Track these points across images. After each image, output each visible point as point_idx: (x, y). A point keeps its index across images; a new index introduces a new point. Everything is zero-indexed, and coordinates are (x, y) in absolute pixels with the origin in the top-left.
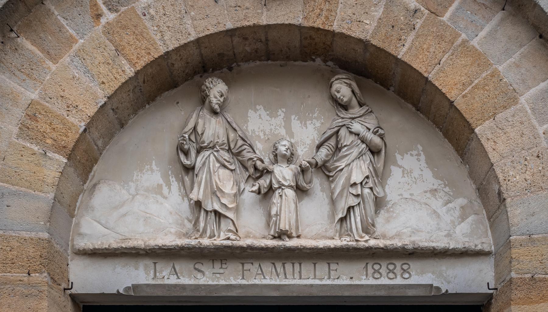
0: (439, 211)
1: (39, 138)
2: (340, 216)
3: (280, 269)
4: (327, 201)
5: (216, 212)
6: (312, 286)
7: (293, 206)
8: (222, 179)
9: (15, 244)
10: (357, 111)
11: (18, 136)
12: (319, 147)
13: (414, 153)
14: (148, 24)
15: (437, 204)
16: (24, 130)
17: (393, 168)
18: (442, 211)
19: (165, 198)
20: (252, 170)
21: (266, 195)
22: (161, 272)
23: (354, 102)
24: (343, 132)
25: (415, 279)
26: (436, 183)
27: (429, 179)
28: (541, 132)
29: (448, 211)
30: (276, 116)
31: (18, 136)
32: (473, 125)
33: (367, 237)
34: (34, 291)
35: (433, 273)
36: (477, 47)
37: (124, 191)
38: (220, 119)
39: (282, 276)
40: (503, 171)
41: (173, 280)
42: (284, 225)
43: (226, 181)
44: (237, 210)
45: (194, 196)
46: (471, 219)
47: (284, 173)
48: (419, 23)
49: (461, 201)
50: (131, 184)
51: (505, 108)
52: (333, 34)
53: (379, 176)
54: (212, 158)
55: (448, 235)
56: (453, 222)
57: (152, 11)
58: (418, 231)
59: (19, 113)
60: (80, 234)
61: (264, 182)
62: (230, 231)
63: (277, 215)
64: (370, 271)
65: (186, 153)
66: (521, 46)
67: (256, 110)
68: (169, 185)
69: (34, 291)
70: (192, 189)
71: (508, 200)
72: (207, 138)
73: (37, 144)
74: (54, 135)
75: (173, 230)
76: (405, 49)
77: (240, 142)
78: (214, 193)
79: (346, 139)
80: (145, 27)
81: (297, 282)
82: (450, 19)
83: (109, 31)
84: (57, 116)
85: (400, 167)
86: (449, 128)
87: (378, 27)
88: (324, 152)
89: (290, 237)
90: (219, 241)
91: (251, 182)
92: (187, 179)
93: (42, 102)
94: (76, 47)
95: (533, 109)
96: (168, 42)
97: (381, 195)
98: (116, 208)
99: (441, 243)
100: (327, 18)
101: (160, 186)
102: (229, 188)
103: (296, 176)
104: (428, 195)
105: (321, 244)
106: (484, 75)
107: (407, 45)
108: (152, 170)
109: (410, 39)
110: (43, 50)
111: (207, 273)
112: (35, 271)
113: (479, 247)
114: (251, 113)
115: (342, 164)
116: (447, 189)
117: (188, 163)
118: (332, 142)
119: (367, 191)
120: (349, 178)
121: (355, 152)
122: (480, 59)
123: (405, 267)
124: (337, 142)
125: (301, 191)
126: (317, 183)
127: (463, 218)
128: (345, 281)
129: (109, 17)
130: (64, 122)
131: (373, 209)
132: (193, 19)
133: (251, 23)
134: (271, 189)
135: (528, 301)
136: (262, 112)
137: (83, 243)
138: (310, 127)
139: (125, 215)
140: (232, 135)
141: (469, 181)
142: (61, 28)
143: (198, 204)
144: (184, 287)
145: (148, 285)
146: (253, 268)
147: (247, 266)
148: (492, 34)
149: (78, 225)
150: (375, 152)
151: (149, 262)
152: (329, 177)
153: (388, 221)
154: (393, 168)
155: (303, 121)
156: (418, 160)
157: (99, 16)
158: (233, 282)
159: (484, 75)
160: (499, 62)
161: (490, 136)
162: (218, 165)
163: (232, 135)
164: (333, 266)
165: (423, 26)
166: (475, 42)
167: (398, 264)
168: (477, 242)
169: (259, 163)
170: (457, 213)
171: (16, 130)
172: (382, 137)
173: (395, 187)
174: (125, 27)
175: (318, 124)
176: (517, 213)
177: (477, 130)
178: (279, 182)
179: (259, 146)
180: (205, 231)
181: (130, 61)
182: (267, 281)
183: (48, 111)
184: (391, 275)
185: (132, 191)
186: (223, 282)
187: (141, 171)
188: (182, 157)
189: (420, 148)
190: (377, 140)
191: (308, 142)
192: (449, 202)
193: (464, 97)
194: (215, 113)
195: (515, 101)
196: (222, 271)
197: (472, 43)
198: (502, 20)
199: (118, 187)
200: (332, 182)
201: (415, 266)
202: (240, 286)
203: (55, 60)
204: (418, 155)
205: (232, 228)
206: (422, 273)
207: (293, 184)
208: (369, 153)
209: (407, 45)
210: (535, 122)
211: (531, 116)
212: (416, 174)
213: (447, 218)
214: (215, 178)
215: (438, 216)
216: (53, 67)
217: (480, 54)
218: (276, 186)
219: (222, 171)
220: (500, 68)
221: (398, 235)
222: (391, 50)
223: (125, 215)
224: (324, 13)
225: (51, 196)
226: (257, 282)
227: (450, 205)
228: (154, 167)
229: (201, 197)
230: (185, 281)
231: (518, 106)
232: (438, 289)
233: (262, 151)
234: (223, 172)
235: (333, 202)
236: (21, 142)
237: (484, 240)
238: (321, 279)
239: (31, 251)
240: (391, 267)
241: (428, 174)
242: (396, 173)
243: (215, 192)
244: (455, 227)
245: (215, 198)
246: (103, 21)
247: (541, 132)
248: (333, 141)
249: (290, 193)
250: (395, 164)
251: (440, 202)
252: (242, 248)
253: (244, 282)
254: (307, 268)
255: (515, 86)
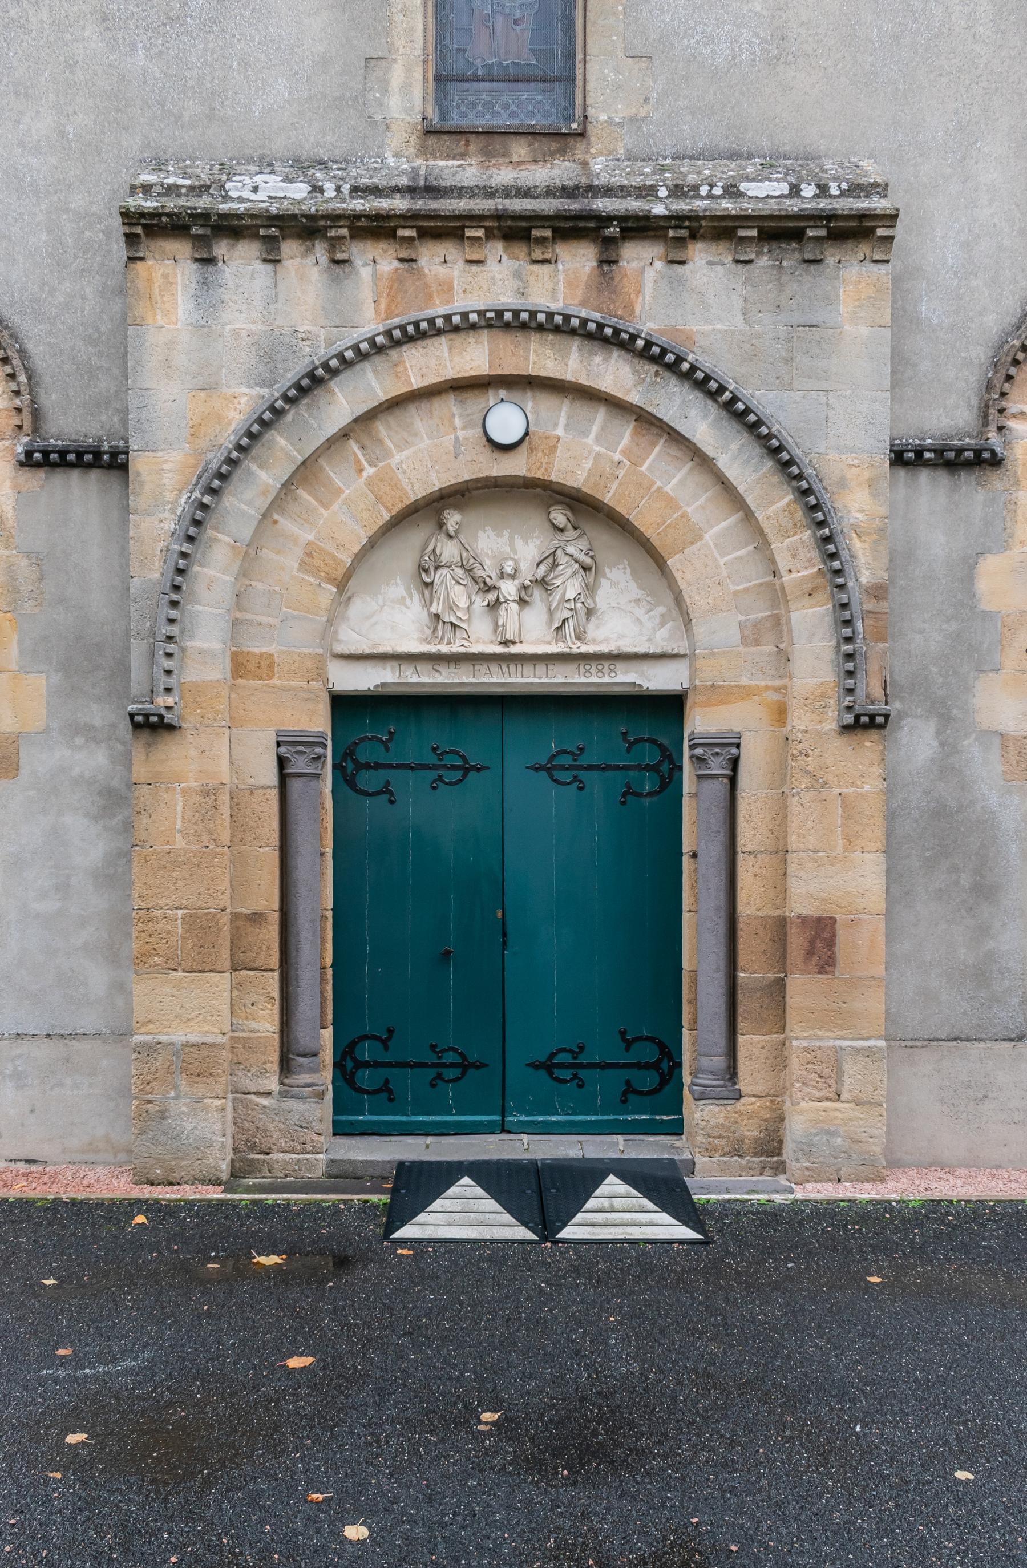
0: (641, 618)
1: (315, 572)
2: (557, 625)
3: (505, 669)
4: (545, 609)
5: (452, 623)
6: (532, 683)
7: (517, 617)
8: (457, 594)
9: (297, 658)
10: (571, 534)
11: (299, 570)
12: (538, 564)
13: (621, 566)
14: (401, 476)
15: (640, 612)
16: (303, 564)
17: (603, 580)
18: (644, 618)
19: (408, 608)
20: (482, 585)
21: (494, 606)
22: (405, 672)
23: (569, 526)
24: (559, 552)
25: (621, 678)
26: (638, 593)
27: (634, 591)
28: (722, 563)
29: (650, 618)
30: (502, 536)
31: (299, 570)
32: (666, 558)
33: (579, 644)
34: (312, 696)
35: (636, 673)
36: (670, 492)
37: (374, 603)
38: (455, 541)
39: (506, 675)
40: (690, 597)
41: (415, 679)
42: (509, 636)
43: (460, 596)
44: (469, 620)
45: (434, 609)
46: (669, 625)
47: (509, 589)
48: (621, 473)
49: (661, 609)
50: (379, 596)
51: (692, 543)
52: (551, 482)
53: (590, 589)
54: (449, 576)
55: (649, 640)
56: (653, 628)
57: (404, 466)
58: (623, 636)
59: (299, 552)
60: (338, 641)
61: (492, 596)
62: (464, 639)
63: (503, 626)
64: (582, 670)
65: (426, 571)
66: (706, 491)
67: (485, 531)
68: (411, 597)
69: (312, 696)
70: (431, 603)
71: (694, 621)
72: (444, 559)
73: (313, 576)
74: (327, 569)
75: (415, 637)
76: (610, 495)
77: (472, 561)
78: (451, 608)
79: (562, 559)
80: (399, 480)
81: (519, 680)
82: (649, 468)
83: (370, 483)
84: (329, 554)
85: (609, 579)
86: (650, 555)
87: (588, 476)
88: (543, 568)
89: (514, 643)
90: (455, 648)
91: (481, 594)
92: (427, 593)
93: (316, 542)
94: (343, 496)
95: (716, 545)
96: (417, 492)
97: (592, 606)
98: (368, 618)
99: (641, 649)
100: (546, 470)
101: (404, 598)
102: (463, 603)
103: (519, 591)
104: (633, 604)
105: (541, 649)
106: (675, 516)
107: (612, 492)
108: (397, 584)
109: (614, 487)
110: (316, 499)
111: (443, 673)
112: (313, 680)
113: (676, 651)
114: (480, 533)
115: (558, 582)
116: (649, 599)
117: (428, 580)
118: (550, 560)
119: (579, 605)
120: (564, 594)
121: (569, 572)
122: (671, 503)
123: (612, 667)
124: (554, 561)
125: (522, 602)
126: (537, 593)
127: (662, 624)
128: (560, 679)
129: (369, 471)
130: (334, 558)
131: (584, 619)
132: (438, 472)
133: (484, 475)
134: (497, 603)
135: (709, 704)
136: (490, 532)
137: (339, 649)
138: (531, 545)
139: (375, 624)
140: (465, 554)
141: (668, 591)
142: (331, 481)
143: (437, 617)
144: (423, 685)
145: (394, 683)
146: (482, 668)
147: (477, 667)
148: (682, 483)
149: (336, 632)
150: (586, 569)
151: (395, 664)
152: (547, 590)
153: (597, 627)
154: (603, 580)
155: (525, 539)
156: (625, 573)
157: (361, 470)
158: (466, 681)
159: (675, 516)
160: (688, 505)
161: (679, 567)
162: (453, 582)
163: (465, 554)
164: (550, 667)
165: (625, 476)
166: (668, 489)
167: (606, 665)
168: (675, 646)
169: (488, 580)
170: (657, 620)
171: (296, 565)
172: (592, 557)
173: (605, 596)
174: (381, 480)
175: (538, 542)
176: (700, 630)
177: (668, 562)
178: (505, 597)
179: (487, 562)
180: (442, 638)
181: (386, 507)
182: (494, 680)
183: (322, 550)
184: (600, 674)
185: (381, 602)
186: (457, 681)
187: (388, 585)
188: (424, 575)
189: (626, 562)
190: (588, 561)
191: (530, 558)
192: (651, 610)
193: (658, 534)
194: (450, 537)
195: (700, 537)
196: (456, 671)
197: (665, 489)
198: (691, 469)
199: (369, 599)
200: (550, 595)
201: (620, 666)
202: (471, 684)
203: (326, 507)
204: (625, 568)
205: (466, 636)
206: (627, 672)
207: (517, 598)
208: (581, 570)
209: (612, 492)
210: (717, 555)
211: (715, 551)
212: (622, 586)
213: (649, 625)
214: (452, 594)
215: (641, 623)
216: (325, 513)
217: (672, 498)
218: (502, 600)
219: (457, 588)
220: (689, 510)
221: (606, 640)
222: (598, 496)
223: (375, 624)
224: (544, 465)
225: (325, 619)
226: (486, 680)
227: (652, 613)
228: (399, 581)
229: (440, 611)
230: (425, 679)
231: (704, 542)
232: (640, 686)
233: (489, 571)
234: (458, 588)
235: (551, 613)
236: (300, 575)
237: (680, 644)
238: (540, 678)
239: (310, 664)
240: (600, 667)
241: (633, 585)
242: (604, 583)
243: (451, 607)
244: (655, 631)
245: (452, 612)
246: (365, 474)
247: (722, 563)
248: (551, 560)
249: (514, 606)
250: (605, 576)
251: (643, 611)
252: (474, 654)
253: (474, 680)
254: (528, 669)
255: (701, 525)
